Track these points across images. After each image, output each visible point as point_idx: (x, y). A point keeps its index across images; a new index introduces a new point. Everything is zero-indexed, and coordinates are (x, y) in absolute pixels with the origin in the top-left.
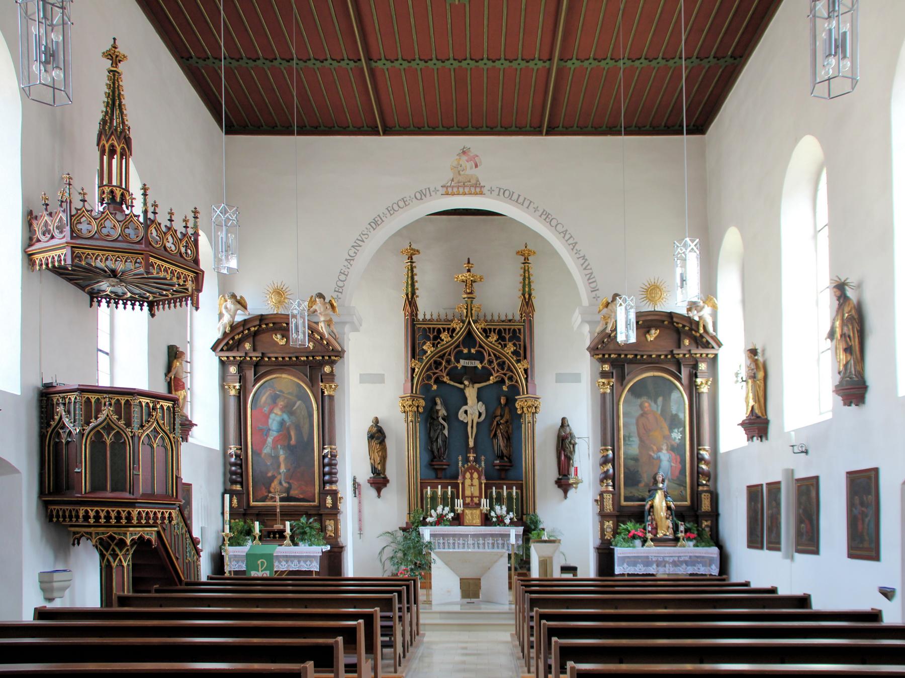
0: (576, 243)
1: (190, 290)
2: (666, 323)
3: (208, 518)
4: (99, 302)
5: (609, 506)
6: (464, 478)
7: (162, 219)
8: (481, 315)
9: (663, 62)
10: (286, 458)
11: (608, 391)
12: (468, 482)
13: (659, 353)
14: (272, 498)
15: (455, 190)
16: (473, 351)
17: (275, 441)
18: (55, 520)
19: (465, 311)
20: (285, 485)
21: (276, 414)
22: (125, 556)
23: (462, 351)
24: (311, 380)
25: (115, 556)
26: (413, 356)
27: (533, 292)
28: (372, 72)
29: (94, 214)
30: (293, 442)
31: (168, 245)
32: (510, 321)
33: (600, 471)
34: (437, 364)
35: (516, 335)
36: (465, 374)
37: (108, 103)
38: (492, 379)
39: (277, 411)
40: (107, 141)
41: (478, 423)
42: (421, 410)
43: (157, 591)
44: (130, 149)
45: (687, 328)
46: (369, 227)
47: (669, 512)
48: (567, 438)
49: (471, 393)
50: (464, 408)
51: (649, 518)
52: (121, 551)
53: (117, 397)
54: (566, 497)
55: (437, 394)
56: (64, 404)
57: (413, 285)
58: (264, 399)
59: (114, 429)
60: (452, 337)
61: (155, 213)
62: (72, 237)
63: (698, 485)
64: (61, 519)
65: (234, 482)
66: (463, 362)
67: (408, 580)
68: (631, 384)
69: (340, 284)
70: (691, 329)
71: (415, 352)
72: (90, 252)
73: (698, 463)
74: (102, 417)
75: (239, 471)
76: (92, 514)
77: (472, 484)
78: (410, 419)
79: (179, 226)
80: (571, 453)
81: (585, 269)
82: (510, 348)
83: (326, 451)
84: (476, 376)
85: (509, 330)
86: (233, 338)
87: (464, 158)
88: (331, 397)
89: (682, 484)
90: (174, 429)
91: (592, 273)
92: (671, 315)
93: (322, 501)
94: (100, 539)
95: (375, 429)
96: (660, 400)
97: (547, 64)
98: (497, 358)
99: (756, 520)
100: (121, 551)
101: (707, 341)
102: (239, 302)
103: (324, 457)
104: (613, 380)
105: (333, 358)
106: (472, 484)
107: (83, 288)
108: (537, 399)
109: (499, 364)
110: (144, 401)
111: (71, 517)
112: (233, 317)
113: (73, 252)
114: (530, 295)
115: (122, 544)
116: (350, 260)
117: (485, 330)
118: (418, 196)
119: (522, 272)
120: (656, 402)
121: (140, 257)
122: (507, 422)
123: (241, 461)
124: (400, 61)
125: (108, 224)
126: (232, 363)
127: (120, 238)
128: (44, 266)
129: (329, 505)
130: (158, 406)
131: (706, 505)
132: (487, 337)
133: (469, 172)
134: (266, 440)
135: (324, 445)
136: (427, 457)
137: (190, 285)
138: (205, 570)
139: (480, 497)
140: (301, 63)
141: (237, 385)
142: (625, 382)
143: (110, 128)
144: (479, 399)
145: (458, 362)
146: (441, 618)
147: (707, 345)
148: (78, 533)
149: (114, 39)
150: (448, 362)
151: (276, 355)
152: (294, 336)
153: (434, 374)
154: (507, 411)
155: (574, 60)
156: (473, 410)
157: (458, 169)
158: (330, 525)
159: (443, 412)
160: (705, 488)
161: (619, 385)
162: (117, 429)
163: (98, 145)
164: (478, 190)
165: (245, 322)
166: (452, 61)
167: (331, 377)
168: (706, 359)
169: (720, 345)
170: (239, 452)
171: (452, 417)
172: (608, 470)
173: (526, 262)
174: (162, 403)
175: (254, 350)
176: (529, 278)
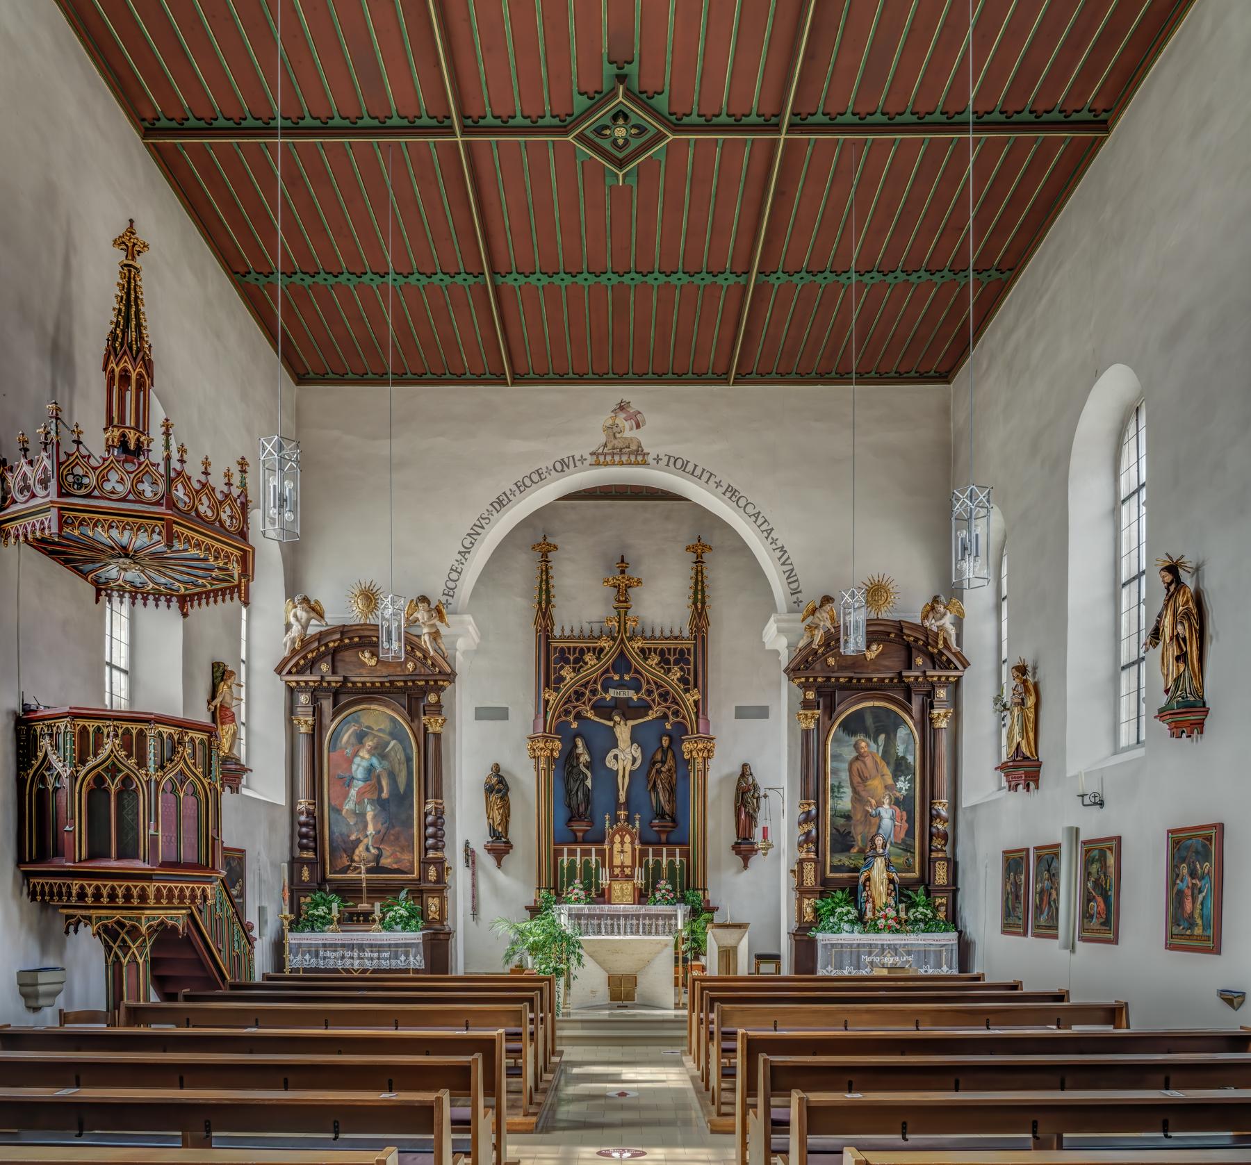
0: (772, 529)
1: (236, 576)
3: (265, 900)
4: (110, 596)
5: (810, 880)
6: (612, 843)
7: (194, 470)
8: (639, 628)
9: (902, 277)
10: (375, 817)
11: (812, 726)
12: (617, 847)
14: (356, 868)
15: (609, 458)
16: (627, 678)
17: (360, 793)
18: (39, 898)
20: (373, 851)
21: (363, 758)
22: (142, 947)
24: (410, 713)
25: (125, 948)
26: (547, 685)
28: (496, 289)
29: (93, 462)
30: (385, 795)
31: (202, 509)
32: (676, 638)
33: (799, 832)
34: (579, 695)
35: (688, 657)
37: (120, 310)
38: (652, 715)
39: (364, 753)
40: (117, 365)
42: (556, 754)
43: (188, 998)
44: (150, 376)
45: (921, 643)
46: (491, 508)
47: (891, 887)
48: (749, 790)
49: (623, 732)
50: (615, 751)
51: (864, 894)
52: (134, 942)
53: (126, 725)
54: (746, 867)
55: (577, 734)
56: (51, 735)
58: (345, 738)
59: (120, 771)
60: (598, 658)
61: (182, 461)
62: (60, 495)
63: (931, 851)
64: (47, 898)
65: (303, 848)
67: (542, 980)
68: (843, 716)
69: (451, 584)
70: (927, 644)
71: (548, 678)
72: (86, 515)
73: (931, 821)
74: (103, 754)
75: (312, 833)
76: (90, 891)
79: (217, 481)
81: (783, 564)
82: (676, 673)
83: (429, 807)
84: (628, 710)
85: (675, 649)
87: (622, 415)
88: (438, 736)
89: (908, 849)
90: (210, 772)
91: (792, 570)
92: (900, 626)
94: (104, 925)
95: (494, 780)
96: (882, 737)
97: (742, 280)
98: (659, 686)
99: (1017, 897)
100: (134, 942)
101: (948, 659)
102: (313, 609)
103: (426, 815)
104: (819, 712)
105: (441, 683)
106: (623, 850)
107: (84, 575)
108: (710, 739)
109: (660, 695)
110: (166, 730)
111: (60, 894)
112: (305, 627)
113: (60, 517)
114: (703, 603)
115: (134, 932)
117: (642, 650)
118: (559, 467)
119: (693, 573)
120: (876, 741)
121: (159, 523)
122: (669, 770)
123: (315, 821)
124: (538, 275)
125: (114, 476)
127: (131, 497)
128: (21, 538)
129: (432, 878)
130: (187, 739)
132: (646, 659)
133: (628, 434)
134: (348, 792)
135: (426, 798)
136: (563, 814)
137: (235, 569)
138: (261, 963)
139: (633, 867)
140: (399, 278)
141: (310, 720)
142: (834, 716)
143: (122, 345)
145: (606, 692)
146: (583, 1029)
147: (948, 665)
148: (73, 916)
149: (131, 221)
150: (594, 692)
151: (363, 679)
152: (386, 645)
153: (575, 707)
154: (670, 754)
155: (780, 274)
156: (625, 757)
157: (612, 431)
158: (433, 903)
159: (585, 758)
160: (940, 855)
162: (126, 771)
163: (105, 369)
164: (640, 458)
165: (320, 637)
166: (610, 275)
168: (946, 683)
169: (965, 664)
170: (312, 807)
171: (597, 763)
172: (809, 832)
174: (192, 734)
175: (334, 672)
176: (702, 582)
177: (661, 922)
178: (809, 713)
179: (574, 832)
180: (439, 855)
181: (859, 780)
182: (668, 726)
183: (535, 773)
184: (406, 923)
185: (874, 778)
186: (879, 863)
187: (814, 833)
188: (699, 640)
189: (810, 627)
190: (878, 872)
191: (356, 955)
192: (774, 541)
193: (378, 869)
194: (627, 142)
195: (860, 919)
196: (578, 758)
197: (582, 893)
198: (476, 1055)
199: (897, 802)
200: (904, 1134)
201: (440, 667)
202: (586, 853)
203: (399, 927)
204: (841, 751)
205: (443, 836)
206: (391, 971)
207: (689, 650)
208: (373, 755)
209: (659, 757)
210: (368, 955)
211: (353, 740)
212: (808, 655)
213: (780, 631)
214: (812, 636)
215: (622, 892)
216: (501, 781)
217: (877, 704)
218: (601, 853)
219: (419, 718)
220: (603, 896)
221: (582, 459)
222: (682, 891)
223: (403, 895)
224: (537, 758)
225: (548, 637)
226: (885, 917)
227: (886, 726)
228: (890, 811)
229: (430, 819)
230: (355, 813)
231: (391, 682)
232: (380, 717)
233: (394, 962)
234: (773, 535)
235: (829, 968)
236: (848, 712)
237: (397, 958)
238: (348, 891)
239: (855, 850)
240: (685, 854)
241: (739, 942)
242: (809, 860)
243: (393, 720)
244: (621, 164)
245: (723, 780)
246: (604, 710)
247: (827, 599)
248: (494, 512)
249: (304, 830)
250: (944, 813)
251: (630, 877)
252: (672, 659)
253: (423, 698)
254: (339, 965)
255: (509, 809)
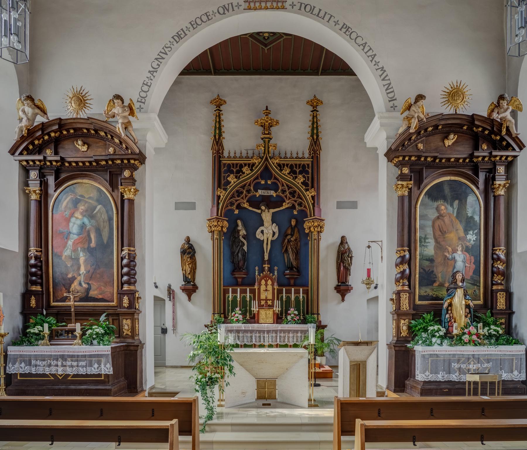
0: (375, 55)
2: (465, 128)
5: (405, 305)
6: (260, 285)
8: (277, 153)
10: (85, 261)
11: (406, 193)
12: (263, 287)
13: (458, 156)
19: (263, 149)
20: (85, 286)
21: (77, 218)
23: (260, 183)
26: (219, 186)
27: (320, 134)
30: (93, 245)
33: (395, 272)
34: (239, 193)
35: (309, 170)
36: (263, 201)
38: (285, 206)
39: (78, 215)
41: (272, 241)
42: (225, 230)
46: (172, 40)
48: (346, 252)
49: (267, 216)
50: (262, 228)
51: (447, 316)
54: (343, 300)
55: (238, 217)
57: (220, 129)
58: (65, 204)
60: (252, 170)
63: (493, 284)
65: (34, 283)
66: (260, 192)
70: (492, 132)
77: (267, 290)
78: (215, 237)
80: (349, 265)
81: (383, 80)
82: (301, 179)
83: (123, 253)
84: (270, 203)
86: (32, 143)
88: (131, 202)
89: (476, 283)
91: (390, 84)
92: (472, 119)
93: (120, 301)
95: (186, 246)
98: (289, 187)
102: (38, 107)
103: (122, 259)
104: (412, 182)
106: (267, 290)
109: (290, 193)
114: (318, 136)
116: (153, 71)
117: (279, 165)
119: (311, 118)
120: (452, 205)
122: (296, 240)
126: (34, 168)
131: (501, 303)
132: (281, 170)
134: (66, 243)
135: (122, 246)
136: (229, 267)
139: (273, 300)
144: (273, 221)
145: (257, 191)
147: (508, 147)
156: (268, 231)
158: (126, 324)
159: (243, 232)
160: (500, 287)
161: (416, 188)
164: (280, 4)
165: (43, 127)
167: (132, 181)
169: (521, 146)
171: (250, 236)
172: (405, 270)
173: (315, 110)
176: (317, 122)
177: (291, 335)
178: (404, 183)
179: (236, 278)
180: (132, 288)
181: (440, 235)
182: (295, 213)
183: (211, 242)
184: (100, 338)
185: (451, 232)
186: (459, 293)
187: (407, 271)
188: (315, 159)
189: (408, 118)
190: (459, 300)
191: (60, 363)
192: (377, 63)
193: (87, 298)
194: (268, 38)
195: (448, 335)
196: (239, 233)
197: (240, 317)
198: (175, 421)
199: (467, 250)
200: (414, 442)
201: (132, 149)
202: (244, 292)
203: (95, 342)
204: (425, 212)
205: (135, 274)
206: (87, 375)
207: (308, 165)
208: (84, 216)
209: (289, 232)
210: (69, 363)
211: (70, 205)
212: (404, 140)
213: (382, 125)
214: (410, 124)
215: (266, 316)
216: (191, 247)
217: (453, 178)
218: (253, 292)
219: (118, 189)
220: (254, 319)
221: (238, 6)
222: (304, 315)
223: (103, 318)
224: (212, 232)
225: (220, 157)
226: (470, 333)
227: (459, 195)
228: (462, 256)
229: (125, 261)
230: (71, 258)
231: (97, 161)
232: (90, 188)
233: (89, 369)
234: (376, 59)
235: (427, 373)
236: (432, 184)
237: (91, 365)
238: (62, 315)
239: (436, 284)
240: (306, 292)
241: (368, 358)
242: (405, 291)
243: (99, 190)
244: (266, 45)
245: (328, 247)
246: (255, 203)
247: (420, 97)
248: (175, 43)
249: (34, 270)
250: (502, 257)
251: (272, 306)
252: (298, 171)
253: (121, 174)
254: (47, 371)
255: (195, 264)
